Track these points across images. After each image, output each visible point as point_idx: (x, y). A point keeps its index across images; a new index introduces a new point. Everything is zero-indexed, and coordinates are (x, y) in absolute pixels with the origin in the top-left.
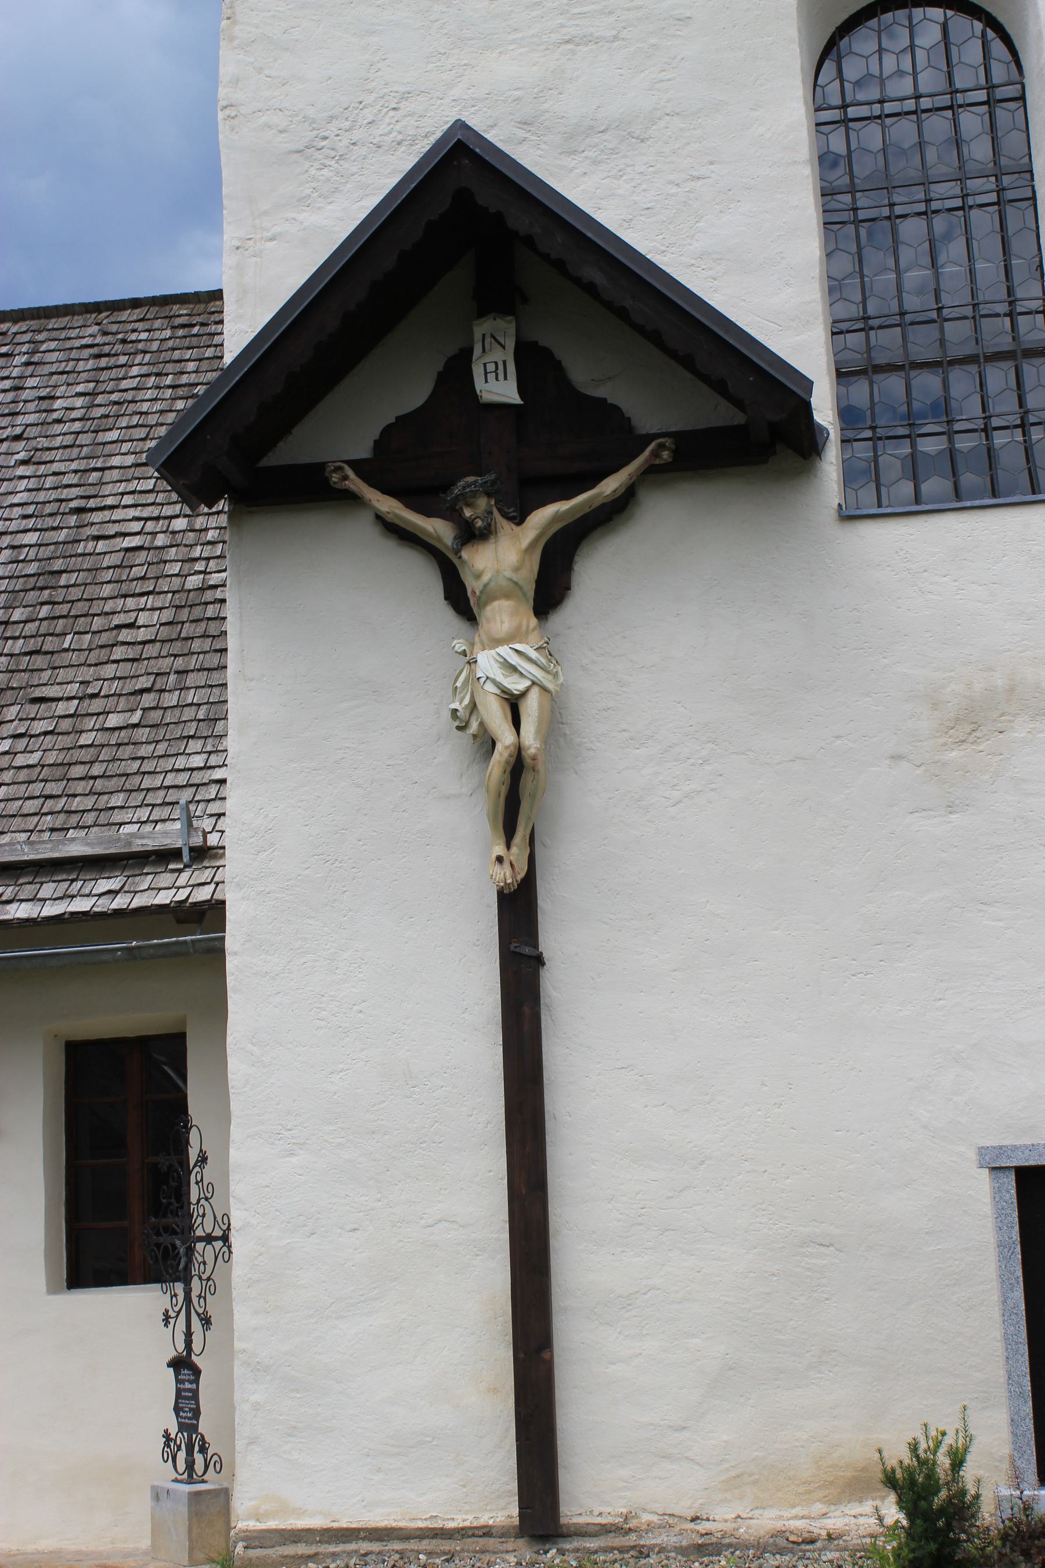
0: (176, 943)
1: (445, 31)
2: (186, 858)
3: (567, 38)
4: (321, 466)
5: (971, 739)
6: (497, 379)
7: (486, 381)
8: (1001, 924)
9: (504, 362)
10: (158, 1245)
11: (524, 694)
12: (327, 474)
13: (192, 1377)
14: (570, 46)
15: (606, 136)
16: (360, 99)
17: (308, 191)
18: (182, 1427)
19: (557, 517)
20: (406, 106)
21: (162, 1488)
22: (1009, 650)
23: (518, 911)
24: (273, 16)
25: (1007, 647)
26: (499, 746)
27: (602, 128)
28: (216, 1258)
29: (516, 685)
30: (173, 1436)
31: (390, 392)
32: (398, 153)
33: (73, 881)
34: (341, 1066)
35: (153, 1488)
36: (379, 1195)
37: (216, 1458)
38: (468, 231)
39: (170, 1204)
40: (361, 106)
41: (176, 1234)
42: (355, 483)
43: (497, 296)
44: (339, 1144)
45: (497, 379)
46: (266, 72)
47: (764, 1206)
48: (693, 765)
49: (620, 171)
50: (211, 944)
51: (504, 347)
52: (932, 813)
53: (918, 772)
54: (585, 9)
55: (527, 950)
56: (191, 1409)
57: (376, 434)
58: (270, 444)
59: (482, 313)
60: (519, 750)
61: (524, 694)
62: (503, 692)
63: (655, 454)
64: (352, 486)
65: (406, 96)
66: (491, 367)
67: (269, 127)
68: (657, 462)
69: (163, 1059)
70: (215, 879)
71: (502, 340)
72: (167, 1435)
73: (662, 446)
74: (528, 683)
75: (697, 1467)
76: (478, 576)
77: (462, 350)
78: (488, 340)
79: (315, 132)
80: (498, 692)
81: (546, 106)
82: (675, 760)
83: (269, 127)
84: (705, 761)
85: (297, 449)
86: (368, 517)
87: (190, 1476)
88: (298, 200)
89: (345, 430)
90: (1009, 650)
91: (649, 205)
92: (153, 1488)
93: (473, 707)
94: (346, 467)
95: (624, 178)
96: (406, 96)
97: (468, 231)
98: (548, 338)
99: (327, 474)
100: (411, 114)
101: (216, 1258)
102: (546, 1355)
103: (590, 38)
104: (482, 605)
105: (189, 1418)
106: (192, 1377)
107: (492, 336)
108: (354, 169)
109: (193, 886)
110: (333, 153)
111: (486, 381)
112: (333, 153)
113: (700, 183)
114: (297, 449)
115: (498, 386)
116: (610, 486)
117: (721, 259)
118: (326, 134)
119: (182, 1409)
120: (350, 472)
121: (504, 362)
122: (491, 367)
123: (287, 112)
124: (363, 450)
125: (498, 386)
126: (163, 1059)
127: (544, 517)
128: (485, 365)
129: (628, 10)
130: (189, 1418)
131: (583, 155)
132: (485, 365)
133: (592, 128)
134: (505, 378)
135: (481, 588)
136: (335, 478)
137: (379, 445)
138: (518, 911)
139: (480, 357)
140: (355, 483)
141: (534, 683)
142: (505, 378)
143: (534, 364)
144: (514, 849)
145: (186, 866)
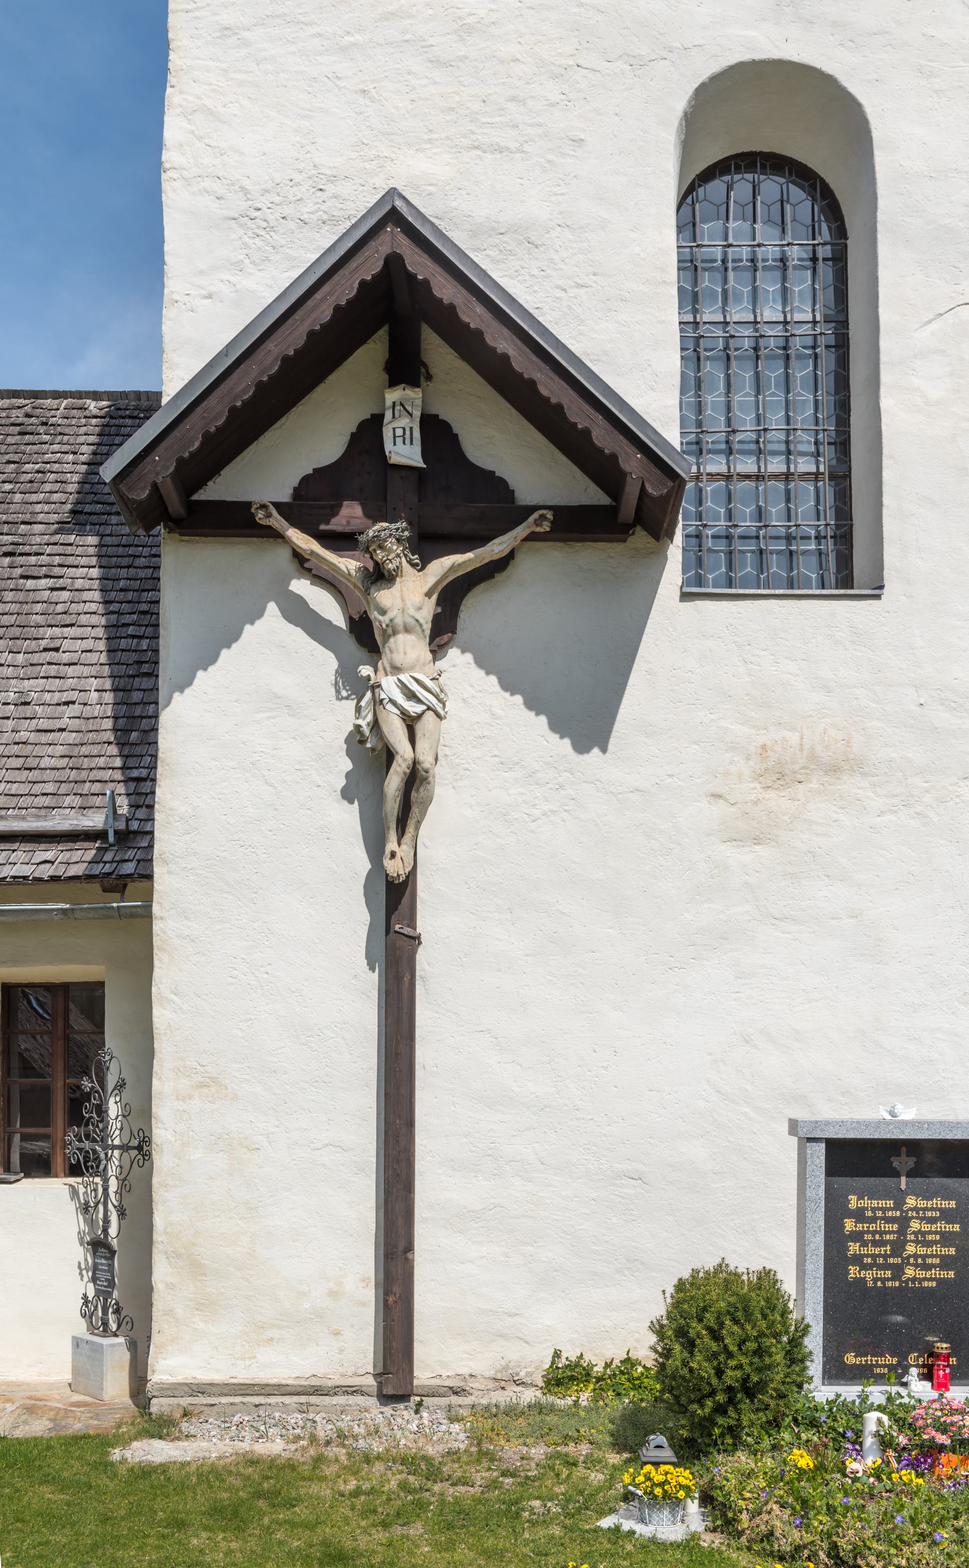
0: (132, 906)
1: (368, 124)
2: (111, 839)
3: (476, 144)
4: (249, 504)
5: (776, 786)
6: (404, 443)
7: (395, 444)
8: (789, 936)
9: (411, 429)
10: (80, 1150)
11: (420, 716)
12: (253, 510)
13: (108, 1255)
14: (479, 152)
15: (505, 238)
16: (291, 177)
17: (242, 257)
18: (98, 1293)
19: (452, 568)
20: (331, 189)
21: (81, 1339)
22: (811, 716)
23: (394, 898)
24: (213, 90)
25: (811, 713)
26: (398, 759)
27: (503, 231)
28: (132, 1163)
29: (414, 708)
30: (90, 1299)
31: (312, 440)
32: (322, 231)
33: (14, 851)
34: (249, 1016)
35: (74, 1338)
36: (277, 1123)
37: (127, 1319)
38: (392, 301)
39: (92, 1117)
40: (291, 184)
41: (97, 1141)
42: (277, 521)
43: (405, 368)
44: (245, 1080)
45: (404, 443)
46: (206, 141)
47: (588, 1147)
48: (551, 789)
49: (516, 271)
50: (134, 910)
51: (411, 415)
52: (740, 843)
53: (733, 809)
54: (493, 120)
55: (407, 931)
56: (107, 1280)
57: (295, 482)
58: (201, 482)
59: (393, 383)
60: (415, 762)
61: (420, 716)
62: (402, 713)
63: (537, 523)
64: (275, 523)
65: (333, 179)
66: (399, 432)
67: (207, 192)
68: (538, 529)
69: (935, 1339)
70: (137, 857)
71: (409, 409)
72: (85, 1297)
73: (543, 517)
74: (425, 707)
75: (525, 1345)
76: (383, 612)
77: (363, 425)
78: (398, 408)
79: (250, 203)
80: (398, 713)
81: (454, 204)
82: (537, 784)
83: (207, 192)
84: (561, 787)
85: (222, 488)
86: (284, 554)
87: (105, 1330)
88: (232, 265)
89: (269, 473)
90: (811, 716)
91: (539, 305)
92: (74, 1338)
93: (375, 725)
94: (271, 507)
95: (519, 278)
96: (333, 179)
97: (392, 301)
98: (446, 412)
99: (253, 510)
100: (335, 197)
101: (132, 1163)
102: (409, 1255)
103: (496, 147)
104: (386, 637)
105: (105, 1287)
106: (108, 1255)
107: (401, 404)
108: (283, 242)
109: (118, 862)
110: (265, 224)
111: (395, 444)
112: (265, 224)
113: (583, 291)
114: (222, 488)
115: (404, 451)
116: (497, 548)
117: (598, 360)
118: (259, 206)
119: (98, 1279)
120: (275, 513)
121: (411, 429)
122: (399, 432)
123: (224, 181)
124: (285, 495)
125: (404, 451)
126: (935, 1339)
127: (444, 565)
128: (394, 429)
129: (531, 125)
130: (105, 1287)
131: (484, 253)
132: (394, 429)
133: (493, 229)
134: (411, 443)
135: (388, 622)
136: (260, 514)
137: (298, 492)
138: (394, 898)
139: (390, 422)
140: (277, 521)
141: (429, 708)
142: (411, 443)
143: (436, 433)
144: (404, 847)
145: (111, 845)
